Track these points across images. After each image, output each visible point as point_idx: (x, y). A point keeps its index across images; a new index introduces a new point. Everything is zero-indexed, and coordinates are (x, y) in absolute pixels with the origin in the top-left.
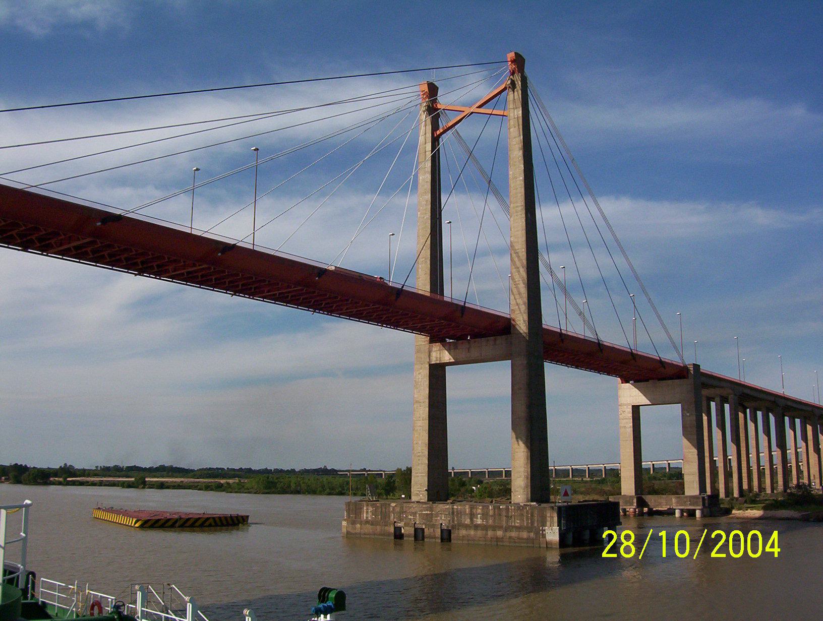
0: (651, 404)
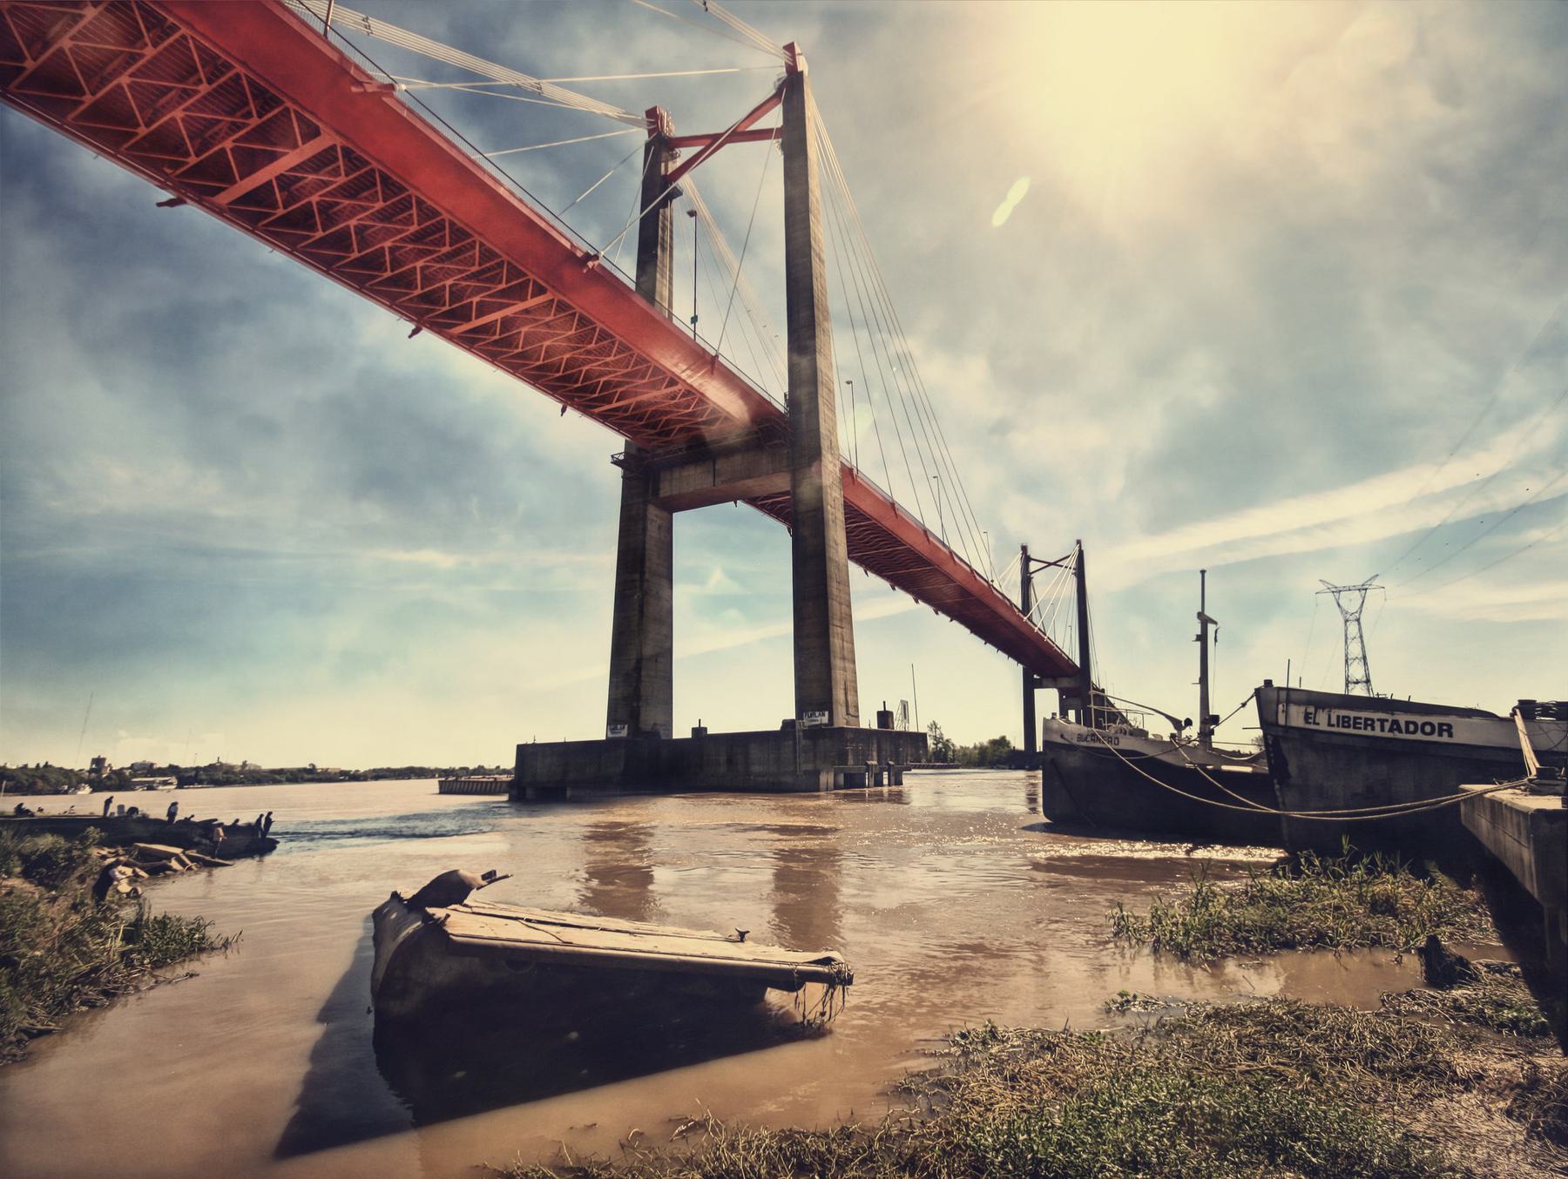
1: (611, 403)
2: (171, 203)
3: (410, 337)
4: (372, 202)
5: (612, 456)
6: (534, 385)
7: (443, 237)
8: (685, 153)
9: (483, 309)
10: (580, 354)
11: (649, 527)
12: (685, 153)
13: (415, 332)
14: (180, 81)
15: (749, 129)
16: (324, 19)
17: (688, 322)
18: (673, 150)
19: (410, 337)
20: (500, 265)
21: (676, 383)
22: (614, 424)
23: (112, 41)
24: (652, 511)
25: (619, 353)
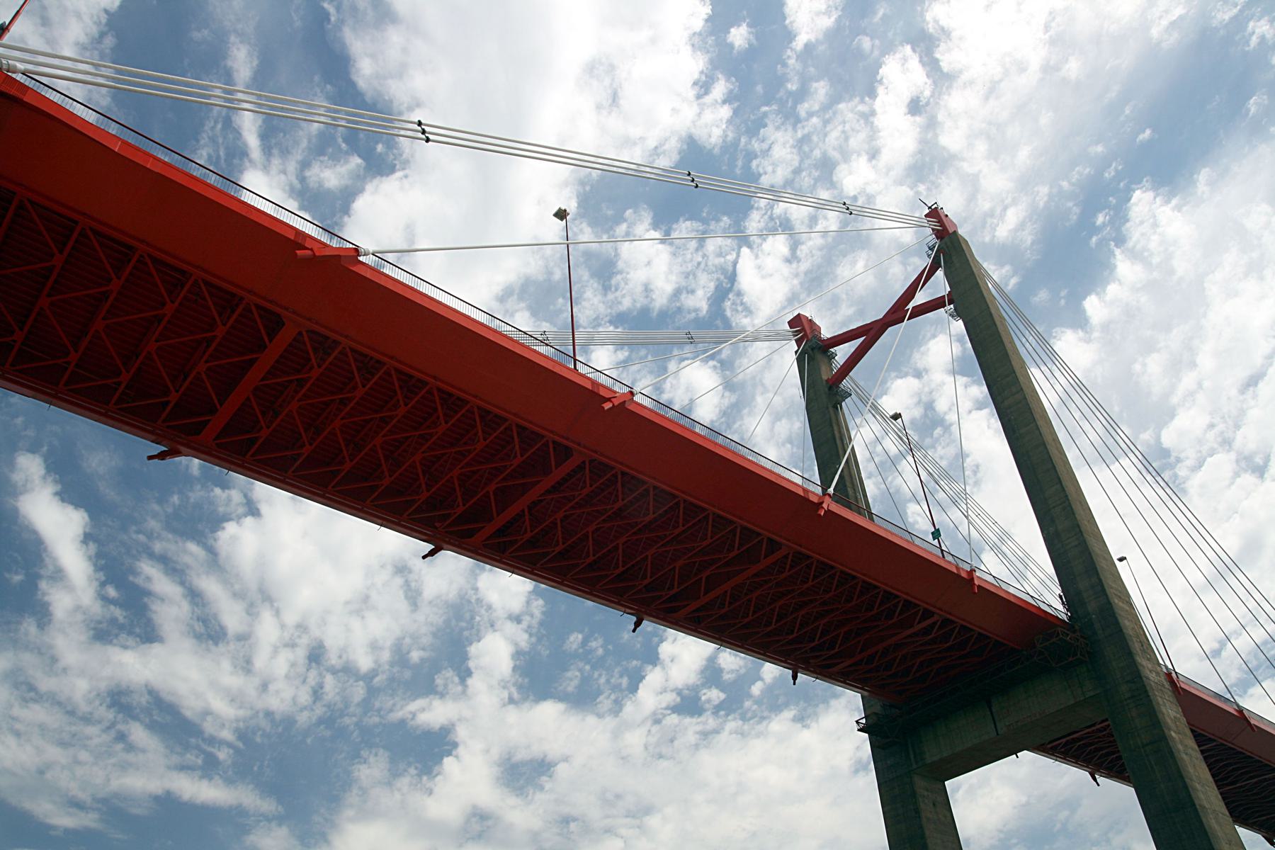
0: (820, 484)
2: (161, 456)
8: (842, 353)
11: (922, 806)
12: (842, 353)
13: (637, 624)
15: (351, 268)
16: (572, 355)
17: (930, 538)
24: (920, 784)
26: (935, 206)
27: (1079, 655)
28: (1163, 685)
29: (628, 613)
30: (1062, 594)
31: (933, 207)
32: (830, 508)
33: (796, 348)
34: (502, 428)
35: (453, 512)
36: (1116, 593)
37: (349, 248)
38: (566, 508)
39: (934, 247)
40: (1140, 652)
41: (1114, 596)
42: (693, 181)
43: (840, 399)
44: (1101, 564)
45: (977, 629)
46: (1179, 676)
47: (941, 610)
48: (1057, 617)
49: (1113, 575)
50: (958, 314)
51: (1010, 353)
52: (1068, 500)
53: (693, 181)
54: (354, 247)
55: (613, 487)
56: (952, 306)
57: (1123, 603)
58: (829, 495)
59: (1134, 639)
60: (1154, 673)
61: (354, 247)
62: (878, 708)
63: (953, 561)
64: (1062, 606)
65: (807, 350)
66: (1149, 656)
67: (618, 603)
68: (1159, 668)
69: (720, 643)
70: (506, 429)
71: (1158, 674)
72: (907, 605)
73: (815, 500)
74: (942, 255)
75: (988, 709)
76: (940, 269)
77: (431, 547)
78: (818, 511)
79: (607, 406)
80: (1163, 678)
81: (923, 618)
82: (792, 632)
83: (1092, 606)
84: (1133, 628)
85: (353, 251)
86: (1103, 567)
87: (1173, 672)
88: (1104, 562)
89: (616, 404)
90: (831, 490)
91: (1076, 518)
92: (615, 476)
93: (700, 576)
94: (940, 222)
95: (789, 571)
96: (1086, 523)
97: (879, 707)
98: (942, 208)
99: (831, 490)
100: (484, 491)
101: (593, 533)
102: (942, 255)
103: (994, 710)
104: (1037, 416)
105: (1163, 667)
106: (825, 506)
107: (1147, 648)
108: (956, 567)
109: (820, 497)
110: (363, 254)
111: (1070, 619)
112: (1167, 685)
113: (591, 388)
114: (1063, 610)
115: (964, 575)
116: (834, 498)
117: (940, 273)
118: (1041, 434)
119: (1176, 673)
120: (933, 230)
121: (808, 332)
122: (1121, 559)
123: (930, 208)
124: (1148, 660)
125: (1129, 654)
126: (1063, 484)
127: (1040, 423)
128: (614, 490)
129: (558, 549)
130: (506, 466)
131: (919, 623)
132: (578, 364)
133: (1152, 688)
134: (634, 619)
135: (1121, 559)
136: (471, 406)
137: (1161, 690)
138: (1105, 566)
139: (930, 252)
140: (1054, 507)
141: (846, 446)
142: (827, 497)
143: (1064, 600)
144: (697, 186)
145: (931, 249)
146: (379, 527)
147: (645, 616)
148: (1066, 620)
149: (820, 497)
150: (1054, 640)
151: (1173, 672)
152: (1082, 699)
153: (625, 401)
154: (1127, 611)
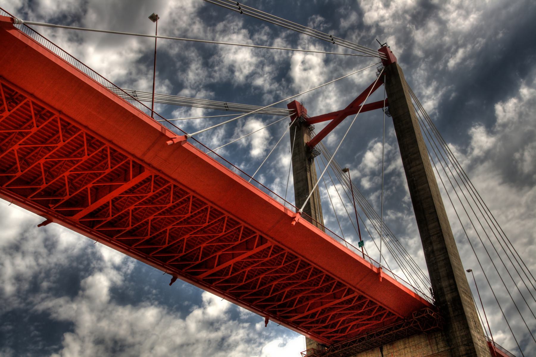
1: (212, 267)
3: (171, 284)
4: (81, 157)
5: (301, 353)
6: (296, 328)
7: (106, 163)
8: (318, 127)
9: (97, 193)
10: (271, 273)
12: (318, 127)
13: (173, 280)
14: (16, 128)
16: (151, 109)
18: (309, 125)
19: (171, 284)
20: (168, 190)
21: (353, 292)
22: (244, 300)
23: (13, 128)
25: (276, 253)
26: (385, 45)
27: (437, 326)
28: (485, 349)
29: (168, 273)
30: (431, 288)
31: (384, 46)
32: (299, 221)
33: (291, 121)
34: (101, 149)
35: (62, 198)
36: (463, 290)
37: (7, 17)
38: (192, 233)
39: (381, 70)
40: (473, 327)
41: (462, 292)
42: (240, 9)
43: (313, 156)
44: (457, 272)
45: (287, 249)
46: (495, 344)
47: (359, 290)
48: (428, 302)
49: (463, 279)
50: (389, 113)
51: (418, 140)
52: (442, 232)
53: (240, 9)
54: (11, 16)
55: (167, 194)
56: (387, 107)
57: (467, 297)
58: (300, 213)
59: (471, 320)
60: (481, 341)
61: (11, 16)
62: (314, 346)
63: (370, 262)
64: (431, 295)
65: (297, 123)
66: (479, 331)
67: (163, 266)
68: (484, 339)
69: (223, 296)
70: (103, 150)
71: (483, 342)
72: (339, 285)
73: (291, 215)
74: (385, 75)
75: (380, 353)
76: (383, 84)
77: (45, 219)
78: (292, 222)
79: (169, 142)
80: (486, 345)
81: (348, 294)
82: (268, 294)
83: (449, 297)
84: (471, 313)
85: (10, 19)
86: (457, 274)
87: (492, 342)
88: (458, 271)
89: (175, 142)
90: (301, 210)
91: (445, 243)
92: (189, 198)
93: (215, 254)
94: (387, 55)
95: (284, 265)
96: (451, 247)
97: (315, 345)
98: (389, 47)
99: (301, 210)
100: (85, 187)
101: (132, 211)
102: (385, 75)
103: (384, 354)
104: (429, 180)
105: (487, 338)
106: (296, 219)
107: (478, 326)
108: (371, 265)
109: (294, 214)
110: (17, 23)
111: (435, 303)
112: (488, 349)
113: (160, 131)
114: (431, 298)
115: (375, 270)
116: (303, 215)
117: (382, 87)
118: (430, 191)
119: (494, 342)
120: (382, 59)
121: (299, 112)
122: (469, 271)
123: (382, 46)
124: (478, 333)
125: (467, 328)
126: (440, 222)
127: (431, 184)
128: (168, 195)
129: (128, 229)
130: (101, 173)
131: (344, 296)
132: (154, 115)
133: (479, 350)
134: (171, 277)
135: (469, 271)
136: (106, 147)
137: (484, 352)
138: (459, 274)
139: (378, 73)
140: (433, 235)
141: (313, 184)
142: (298, 214)
143: (433, 292)
144: (242, 13)
145: (380, 71)
146: (10, 203)
147: (179, 276)
148: (432, 304)
149: (294, 214)
150: (424, 315)
151: (492, 342)
152: (437, 352)
153: (181, 141)
154: (469, 302)
